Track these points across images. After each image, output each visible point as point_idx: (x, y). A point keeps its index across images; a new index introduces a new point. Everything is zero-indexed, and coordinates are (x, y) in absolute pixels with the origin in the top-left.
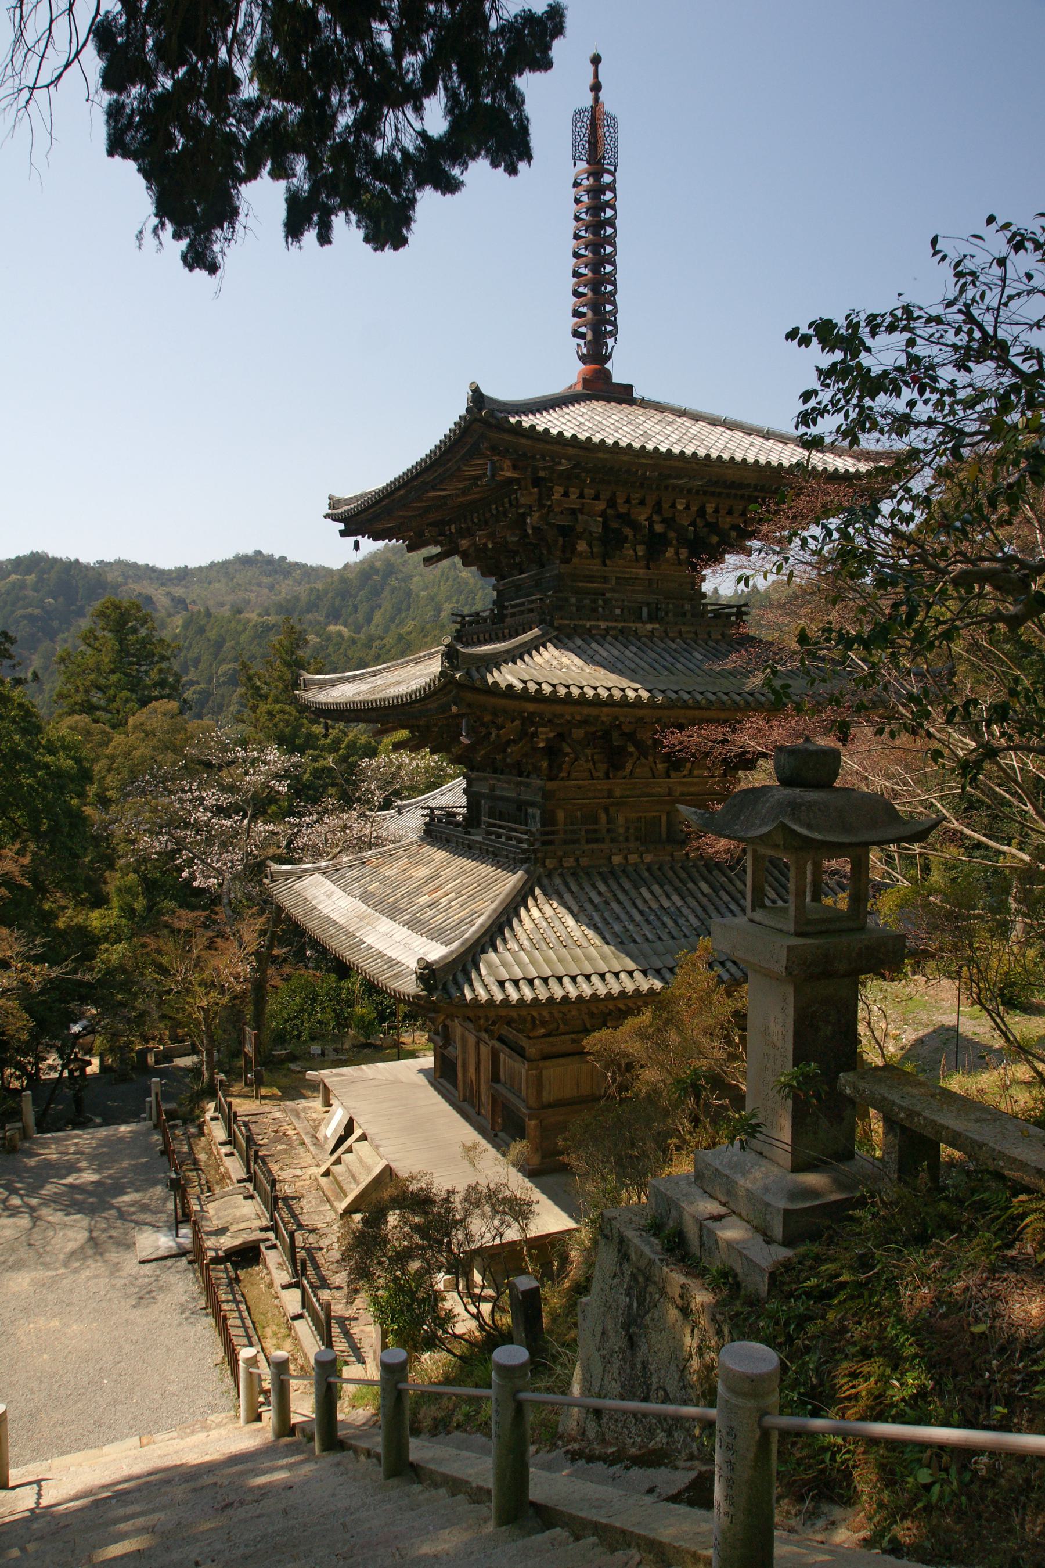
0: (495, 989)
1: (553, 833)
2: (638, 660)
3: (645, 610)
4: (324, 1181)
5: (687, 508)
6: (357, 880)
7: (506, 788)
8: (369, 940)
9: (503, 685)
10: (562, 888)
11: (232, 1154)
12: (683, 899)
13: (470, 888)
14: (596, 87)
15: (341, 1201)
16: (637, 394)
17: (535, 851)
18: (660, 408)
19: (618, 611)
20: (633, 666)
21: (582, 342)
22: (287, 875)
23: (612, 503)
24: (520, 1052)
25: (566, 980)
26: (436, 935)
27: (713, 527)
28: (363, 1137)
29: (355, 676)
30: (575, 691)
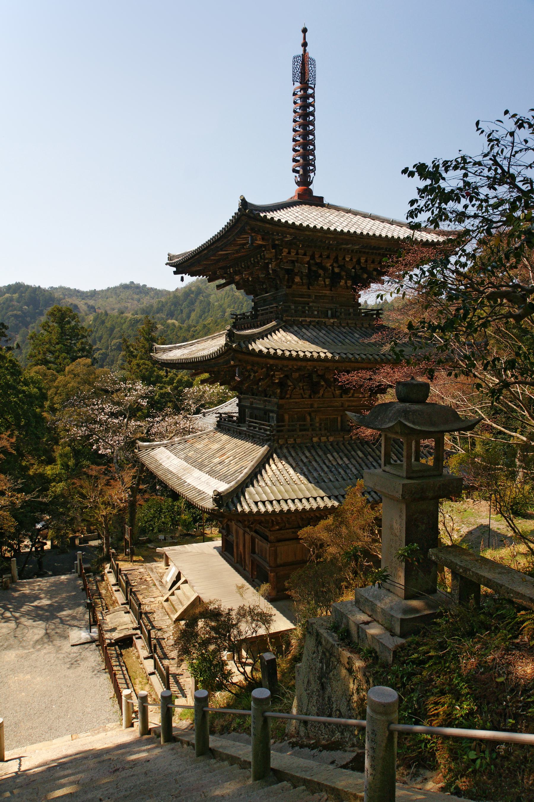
0: (253, 506)
1: (283, 426)
2: (326, 338)
3: (330, 312)
4: (165, 604)
5: (351, 260)
6: (182, 450)
8: (188, 481)
9: (257, 350)
11: (118, 590)
13: (240, 454)
14: (305, 45)
15: (174, 614)
16: (325, 201)
17: (274, 436)
18: (337, 208)
19: (316, 313)
20: (323, 341)
21: (297, 175)
22: (147, 448)
23: (313, 257)
24: (266, 538)
25: (289, 502)
26: (223, 478)
27: (364, 270)
28: (186, 582)
29: (181, 346)
30: (294, 354)
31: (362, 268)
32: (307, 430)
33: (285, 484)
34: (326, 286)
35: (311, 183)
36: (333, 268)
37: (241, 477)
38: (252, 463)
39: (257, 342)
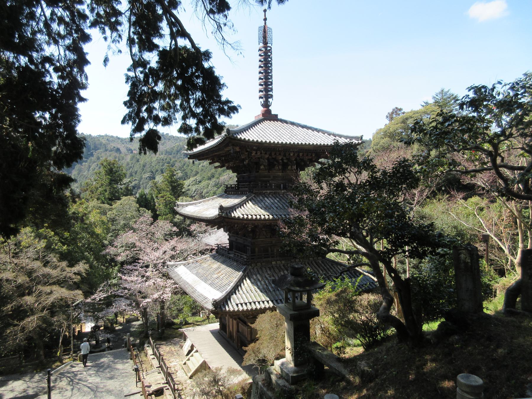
1: (254, 256)
3: (282, 185)
4: (184, 366)
5: (294, 155)
6: (195, 268)
9: (237, 217)
11: (154, 358)
13: (229, 275)
14: (265, 19)
15: (189, 373)
16: (279, 117)
17: (248, 262)
18: (286, 122)
20: (277, 206)
22: (172, 266)
23: (270, 155)
25: (257, 303)
26: (219, 288)
27: (302, 160)
28: (197, 351)
29: (193, 203)
30: (258, 217)
31: (300, 159)
32: (269, 257)
34: (279, 170)
35: (269, 106)
37: (229, 288)
38: (235, 280)
39: (237, 210)
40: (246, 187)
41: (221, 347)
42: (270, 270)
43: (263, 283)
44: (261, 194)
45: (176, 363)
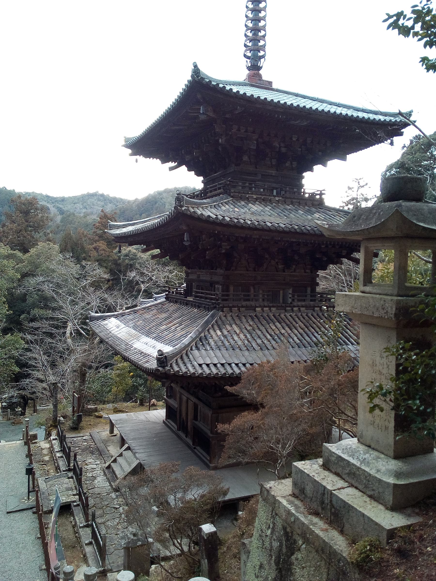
0: (198, 367)
2: (272, 212)
5: (298, 140)
6: (132, 320)
7: (205, 275)
8: (135, 346)
10: (232, 322)
12: (291, 330)
16: (274, 86)
19: (262, 190)
21: (249, 60)
24: (208, 405)
33: (232, 332)
36: (280, 147)
40: (220, 188)
41: (360, 152)
42: (253, 319)
43: (242, 336)
44: (241, 199)
45: (95, 466)
